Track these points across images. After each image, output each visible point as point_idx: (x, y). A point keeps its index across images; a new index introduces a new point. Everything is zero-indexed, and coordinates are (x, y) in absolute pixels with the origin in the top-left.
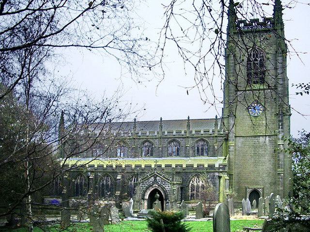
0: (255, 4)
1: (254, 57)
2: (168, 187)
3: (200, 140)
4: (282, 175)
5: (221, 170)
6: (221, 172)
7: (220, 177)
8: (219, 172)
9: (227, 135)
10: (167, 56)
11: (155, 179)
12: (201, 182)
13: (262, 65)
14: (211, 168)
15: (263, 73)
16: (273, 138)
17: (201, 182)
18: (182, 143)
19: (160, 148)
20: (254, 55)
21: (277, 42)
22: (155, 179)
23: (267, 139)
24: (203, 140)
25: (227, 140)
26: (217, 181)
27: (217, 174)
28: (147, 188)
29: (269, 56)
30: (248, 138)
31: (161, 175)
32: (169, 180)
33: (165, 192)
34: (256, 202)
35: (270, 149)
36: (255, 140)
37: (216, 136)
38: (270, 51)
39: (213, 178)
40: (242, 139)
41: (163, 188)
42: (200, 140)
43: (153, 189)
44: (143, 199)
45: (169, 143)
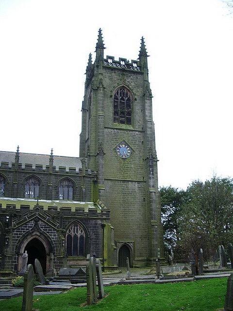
0: (121, 49)
1: (121, 96)
2: (54, 236)
3: (64, 180)
4: (156, 227)
5: (104, 217)
6: (105, 219)
7: (103, 226)
8: (102, 220)
9: (96, 176)
10: (232, 17)
11: (36, 224)
12: (79, 232)
13: (129, 106)
14: (93, 214)
15: (129, 114)
16: (142, 185)
17: (79, 232)
18: (43, 180)
19: (16, 185)
20: (121, 93)
21: (144, 86)
22: (36, 224)
23: (137, 185)
24: (69, 180)
25: (95, 182)
26: (100, 231)
27: (99, 222)
28: (25, 237)
29: (136, 97)
30: (116, 182)
31: (45, 219)
32: (55, 226)
33: (49, 243)
34: (38, 261)
35: (139, 196)
36: (124, 185)
37: (84, 176)
38: (138, 92)
39: (95, 227)
40: (110, 183)
41: (47, 238)
42: (64, 180)
43: (32, 238)
44: (18, 254)
45: (27, 179)
